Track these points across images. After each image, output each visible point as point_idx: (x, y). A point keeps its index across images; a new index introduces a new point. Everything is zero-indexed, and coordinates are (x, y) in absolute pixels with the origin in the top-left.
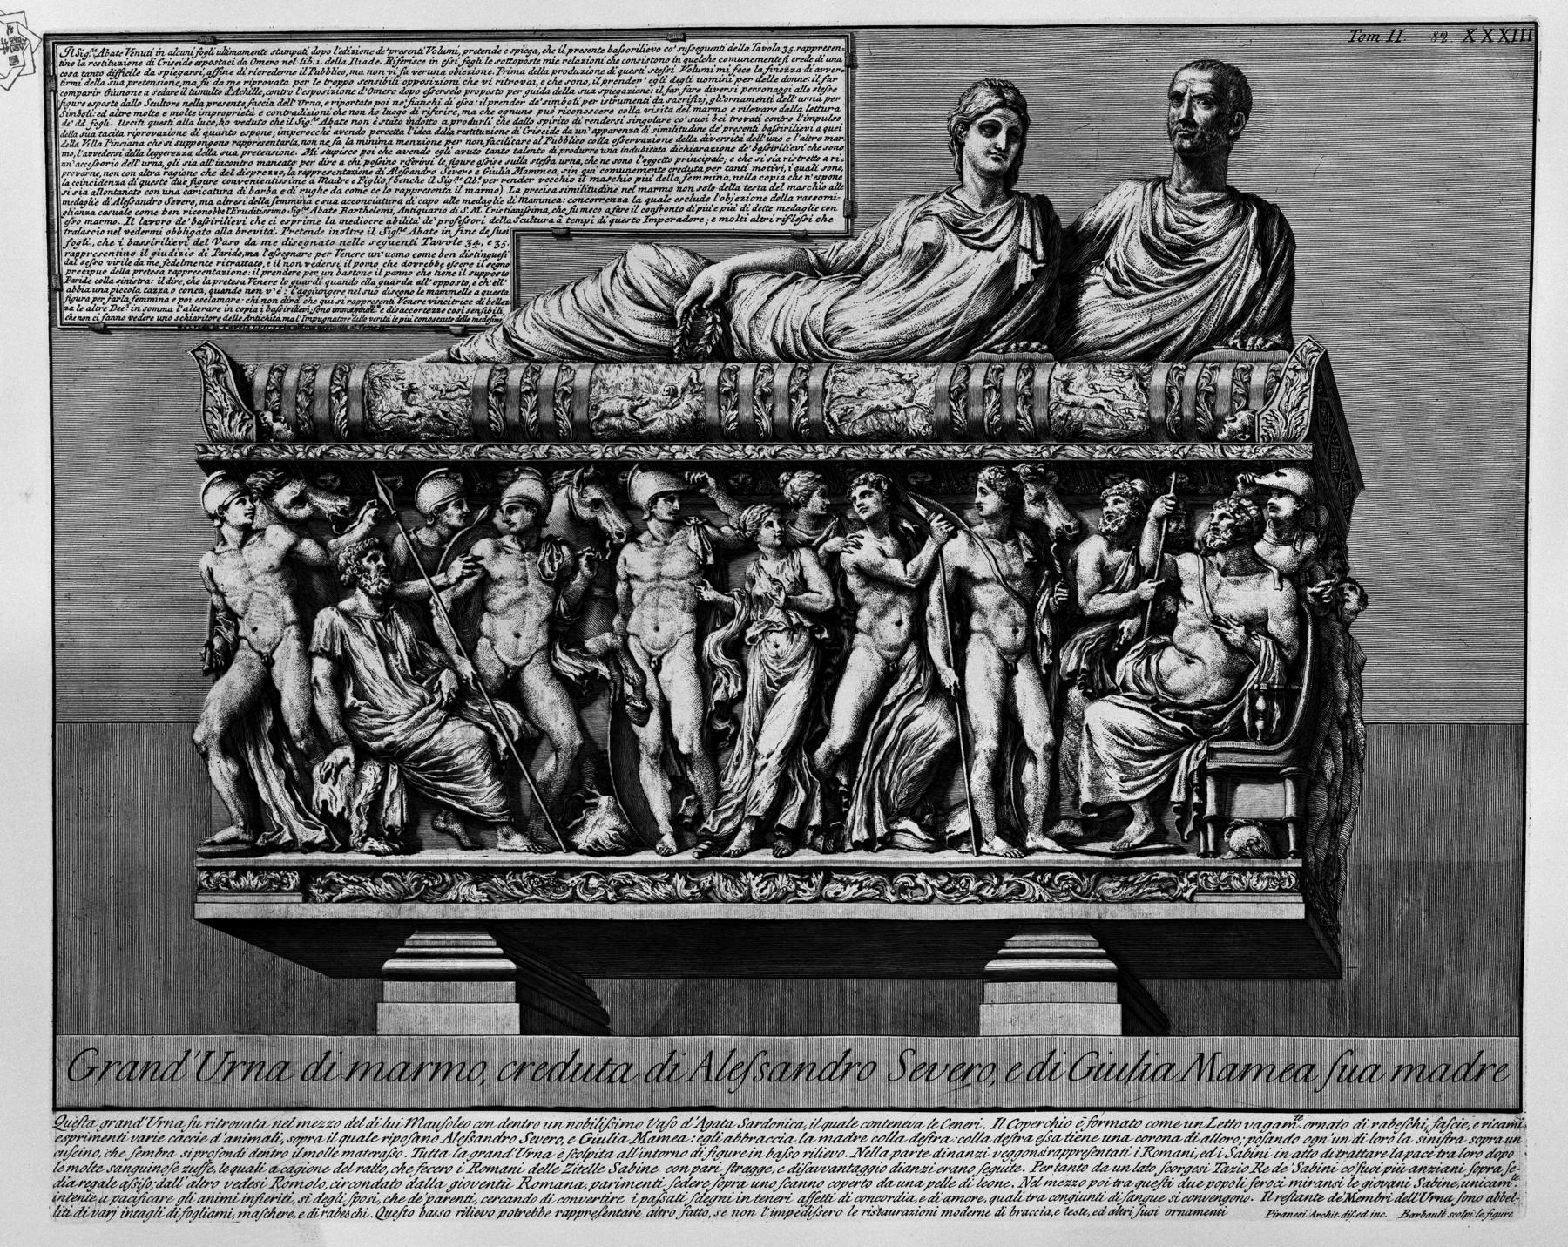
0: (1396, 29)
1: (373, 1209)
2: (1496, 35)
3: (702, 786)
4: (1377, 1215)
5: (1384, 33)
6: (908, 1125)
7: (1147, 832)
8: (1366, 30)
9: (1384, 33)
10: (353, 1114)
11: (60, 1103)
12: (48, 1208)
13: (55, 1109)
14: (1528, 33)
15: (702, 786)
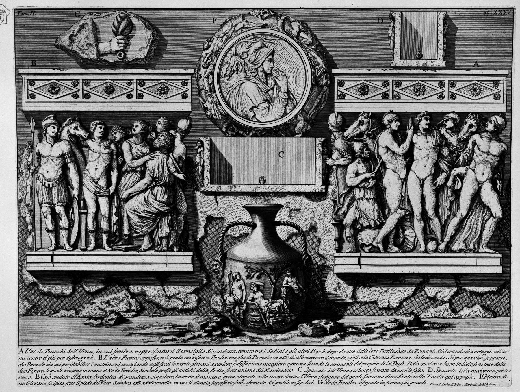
0: (33, 11)
1: (338, 381)
2: (503, 12)
3: (320, 231)
4: (459, 385)
5: (29, 12)
6: (247, 352)
7: (150, 246)
8: (23, 12)
9: (29, 13)
10: (70, 347)
11: (20, 344)
12: (16, 382)
13: (19, 345)
14: (510, 11)
15: (320, 231)
